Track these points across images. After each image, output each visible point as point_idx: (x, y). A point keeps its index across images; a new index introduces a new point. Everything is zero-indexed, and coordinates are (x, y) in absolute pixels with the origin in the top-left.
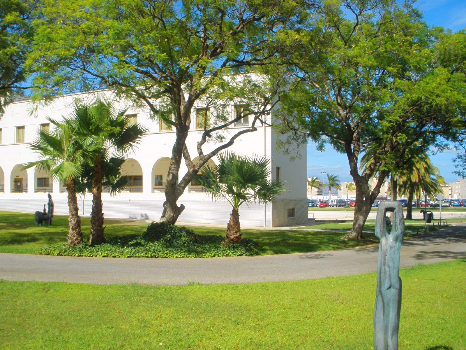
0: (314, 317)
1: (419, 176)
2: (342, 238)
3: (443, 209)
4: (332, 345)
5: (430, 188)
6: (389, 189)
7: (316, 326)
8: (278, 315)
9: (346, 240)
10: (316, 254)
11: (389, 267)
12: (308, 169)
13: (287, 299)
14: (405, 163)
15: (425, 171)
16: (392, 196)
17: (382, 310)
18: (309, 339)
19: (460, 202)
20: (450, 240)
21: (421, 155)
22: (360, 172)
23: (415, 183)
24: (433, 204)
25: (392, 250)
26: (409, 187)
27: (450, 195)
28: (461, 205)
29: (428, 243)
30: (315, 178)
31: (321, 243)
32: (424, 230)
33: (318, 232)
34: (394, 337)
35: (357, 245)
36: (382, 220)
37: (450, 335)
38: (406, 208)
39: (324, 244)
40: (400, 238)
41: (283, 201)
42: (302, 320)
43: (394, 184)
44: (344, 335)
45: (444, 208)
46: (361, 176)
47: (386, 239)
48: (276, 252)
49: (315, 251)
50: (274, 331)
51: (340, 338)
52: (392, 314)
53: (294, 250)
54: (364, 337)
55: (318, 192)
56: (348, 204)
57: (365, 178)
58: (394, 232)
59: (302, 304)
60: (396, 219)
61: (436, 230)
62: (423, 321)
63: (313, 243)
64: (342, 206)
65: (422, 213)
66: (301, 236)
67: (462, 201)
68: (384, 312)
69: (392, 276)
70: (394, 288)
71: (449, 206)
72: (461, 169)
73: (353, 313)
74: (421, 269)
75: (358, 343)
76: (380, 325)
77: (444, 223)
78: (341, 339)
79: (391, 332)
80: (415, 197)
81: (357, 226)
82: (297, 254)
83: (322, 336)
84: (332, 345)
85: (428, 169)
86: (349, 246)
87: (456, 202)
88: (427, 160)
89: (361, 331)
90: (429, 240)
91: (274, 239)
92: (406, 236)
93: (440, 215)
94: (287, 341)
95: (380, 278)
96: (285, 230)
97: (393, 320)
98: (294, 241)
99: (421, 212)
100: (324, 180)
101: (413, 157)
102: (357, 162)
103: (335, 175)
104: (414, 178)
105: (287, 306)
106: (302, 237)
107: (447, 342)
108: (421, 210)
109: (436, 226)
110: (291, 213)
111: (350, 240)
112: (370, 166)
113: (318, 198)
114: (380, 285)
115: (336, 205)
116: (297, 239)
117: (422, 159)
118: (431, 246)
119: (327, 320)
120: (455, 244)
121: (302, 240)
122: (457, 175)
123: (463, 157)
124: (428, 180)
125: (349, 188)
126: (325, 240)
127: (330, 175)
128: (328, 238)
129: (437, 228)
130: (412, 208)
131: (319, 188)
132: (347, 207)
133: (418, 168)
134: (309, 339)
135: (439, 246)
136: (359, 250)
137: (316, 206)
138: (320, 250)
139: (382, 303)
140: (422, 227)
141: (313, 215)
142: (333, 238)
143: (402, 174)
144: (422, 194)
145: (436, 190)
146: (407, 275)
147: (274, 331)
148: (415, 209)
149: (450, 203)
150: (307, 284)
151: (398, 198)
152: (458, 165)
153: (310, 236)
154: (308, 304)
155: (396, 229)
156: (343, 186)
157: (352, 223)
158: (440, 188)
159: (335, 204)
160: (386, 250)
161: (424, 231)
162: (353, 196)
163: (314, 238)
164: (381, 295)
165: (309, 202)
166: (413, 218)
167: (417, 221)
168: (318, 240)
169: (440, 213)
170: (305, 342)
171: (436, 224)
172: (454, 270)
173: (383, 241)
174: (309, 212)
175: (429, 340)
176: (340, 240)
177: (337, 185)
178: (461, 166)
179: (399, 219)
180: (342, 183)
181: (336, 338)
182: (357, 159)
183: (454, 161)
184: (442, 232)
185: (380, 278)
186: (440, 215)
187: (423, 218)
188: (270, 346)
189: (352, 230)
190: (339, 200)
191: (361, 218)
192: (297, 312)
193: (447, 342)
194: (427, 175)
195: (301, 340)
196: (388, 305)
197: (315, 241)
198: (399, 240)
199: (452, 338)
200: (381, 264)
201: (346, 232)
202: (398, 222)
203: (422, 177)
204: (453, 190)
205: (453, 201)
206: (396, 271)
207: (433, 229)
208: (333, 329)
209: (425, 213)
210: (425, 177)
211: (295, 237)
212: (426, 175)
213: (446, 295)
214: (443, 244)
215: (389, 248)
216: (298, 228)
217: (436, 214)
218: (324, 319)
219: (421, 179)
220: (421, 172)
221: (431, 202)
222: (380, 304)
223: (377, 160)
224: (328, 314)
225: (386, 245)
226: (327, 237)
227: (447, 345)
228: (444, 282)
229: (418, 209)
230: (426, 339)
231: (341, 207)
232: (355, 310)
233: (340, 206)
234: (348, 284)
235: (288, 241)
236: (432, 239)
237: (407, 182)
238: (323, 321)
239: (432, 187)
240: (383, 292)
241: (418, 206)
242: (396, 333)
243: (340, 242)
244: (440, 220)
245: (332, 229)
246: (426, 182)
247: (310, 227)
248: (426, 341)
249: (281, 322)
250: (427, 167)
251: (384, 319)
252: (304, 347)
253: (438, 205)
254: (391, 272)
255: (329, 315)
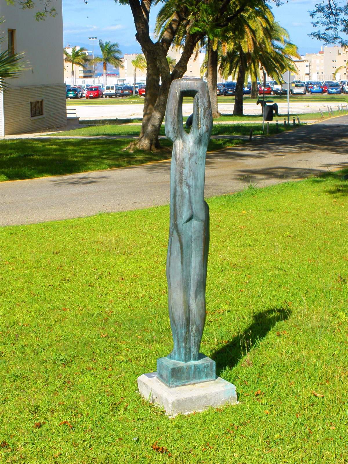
0: (77, 278)
1: (255, 43)
2: (125, 148)
3: (294, 98)
4: (106, 320)
5: (275, 63)
6: (206, 64)
7: (81, 293)
8: (17, 279)
9: (131, 152)
10: (80, 176)
11: (189, 186)
12: (65, 32)
13: (31, 253)
14: (229, 20)
15: (265, 34)
16: (210, 76)
17: (180, 255)
18: (70, 315)
19: (321, 86)
20: (301, 148)
21: (257, 7)
22: (154, 37)
23: (249, 53)
24: (278, 90)
25: (193, 159)
26: (238, 62)
27: (307, 74)
28: (323, 92)
29: (267, 154)
30: (78, 49)
31: (88, 159)
32: (261, 132)
33: (85, 139)
34: (199, 297)
35: (150, 160)
36: (176, 110)
37: (288, 293)
38: (234, 97)
39: (94, 160)
40: (205, 141)
41: (22, 88)
42: (57, 284)
43: (213, 59)
44: (126, 303)
45: (295, 96)
46: (154, 42)
47: (183, 141)
48: (11, 177)
49: (78, 171)
50: (10, 305)
51: (120, 308)
52: (195, 261)
53: (41, 173)
54: (159, 304)
55: (84, 72)
56: (136, 92)
57: (162, 46)
58: (195, 131)
59: (57, 260)
60: (198, 108)
61: (281, 131)
62: (251, 274)
63: (75, 159)
64: (127, 95)
65: (260, 104)
66: (55, 147)
67: (325, 84)
68: (182, 258)
69: (193, 201)
70: (198, 219)
71: (305, 94)
72: (322, 29)
73: (141, 269)
74: (253, 194)
75: (148, 315)
76: (177, 279)
77: (294, 120)
78: (122, 310)
79: (195, 288)
80: (249, 79)
81: (150, 128)
82: (47, 179)
83: (90, 308)
84: (106, 320)
85: (270, 31)
86: (136, 161)
87: (315, 86)
88: (267, 15)
89: (153, 295)
90: (268, 149)
91: (7, 155)
92: (232, 143)
93: (289, 108)
94: (33, 320)
95: (175, 205)
96: (27, 139)
97: (197, 271)
98: (42, 157)
99: (258, 104)
100: (94, 51)
101: (242, 10)
102: (148, 19)
103: (112, 43)
104: (247, 47)
105: (31, 264)
106: (56, 150)
107: (285, 302)
108: (257, 100)
109: (281, 125)
110: (37, 109)
111: (139, 152)
112: (170, 26)
113: (84, 82)
114: (175, 216)
115: (116, 95)
116: (45, 152)
117: (258, 13)
118: (270, 159)
119: (99, 282)
120: (307, 154)
121: (56, 155)
122: (316, 38)
123: (326, 9)
124: (269, 49)
125: (136, 63)
126: (95, 154)
127: (104, 42)
128: (100, 149)
129: (282, 128)
130: (244, 96)
131: (84, 67)
132: (134, 97)
133: (254, 28)
134: (70, 315)
135: (283, 157)
136: (151, 168)
137: (82, 97)
138: (86, 171)
139: (178, 244)
140: (258, 128)
141: (74, 112)
142: (110, 149)
143: (226, 39)
144: (261, 73)
145: (283, 67)
146: (230, 204)
147: (10, 305)
148: (249, 98)
149: (306, 87)
150: (65, 227)
151: (221, 80)
152: (318, 23)
153: (70, 148)
154: (67, 258)
155: (198, 124)
156: (128, 60)
157: (140, 124)
158: (290, 63)
159: (113, 91)
160: (183, 160)
161: (261, 134)
162: (141, 77)
163: (76, 150)
164: (177, 231)
165: (70, 90)
166: (245, 113)
167: (251, 118)
168: (84, 153)
169: (289, 105)
170: (62, 319)
171: (281, 122)
172: (303, 194)
173: (178, 144)
174: (68, 107)
175: (258, 302)
176: (120, 152)
177: (117, 59)
178: (323, 24)
179: (202, 108)
180: (125, 56)
181: (114, 310)
182: (147, 13)
183: (312, 15)
184: (290, 135)
185: (175, 205)
186: (289, 108)
187: (260, 112)
188: (5, 329)
189: (141, 135)
190: (121, 85)
191: (157, 115)
192: (48, 273)
193: (285, 302)
194: (268, 42)
195: (56, 317)
196: (188, 246)
197: (79, 154)
198: (203, 143)
199: (293, 295)
200: (175, 181)
201: (131, 139)
202: (201, 114)
203: (260, 44)
204: (312, 67)
205: (311, 84)
206: (199, 192)
207: (276, 130)
208: (108, 296)
209: (263, 104)
210: (264, 44)
211: (43, 151)
212: (265, 40)
213: (288, 233)
214: (290, 155)
215: (188, 156)
216: (50, 135)
217: (283, 107)
218: (93, 281)
219: (259, 48)
220: (257, 36)
221: (275, 87)
222: (176, 246)
223: (183, 13)
224: (100, 273)
225: (182, 151)
226: (99, 148)
227: (285, 307)
228: (288, 212)
229: (253, 98)
230: (254, 300)
231: (124, 97)
232: (144, 265)
233: (122, 95)
234: (134, 223)
235: (32, 157)
236: (273, 148)
237: (234, 52)
238: (92, 284)
239: (277, 61)
240: (180, 227)
241: (253, 92)
242: (202, 290)
243: (121, 155)
244: (288, 115)
245: (109, 135)
246: (267, 52)
247: (71, 132)
248: (255, 304)
249: (23, 290)
250: (269, 27)
251: (182, 269)
252: (61, 327)
253: (285, 92)
254: (192, 194)
255: (102, 274)
